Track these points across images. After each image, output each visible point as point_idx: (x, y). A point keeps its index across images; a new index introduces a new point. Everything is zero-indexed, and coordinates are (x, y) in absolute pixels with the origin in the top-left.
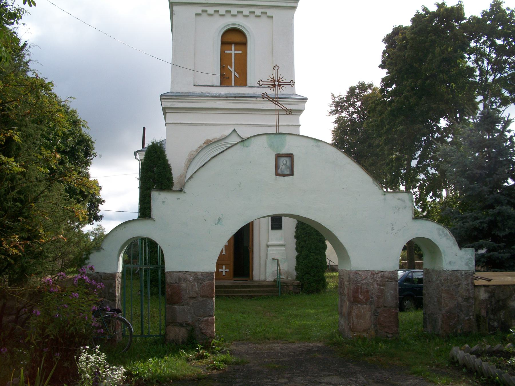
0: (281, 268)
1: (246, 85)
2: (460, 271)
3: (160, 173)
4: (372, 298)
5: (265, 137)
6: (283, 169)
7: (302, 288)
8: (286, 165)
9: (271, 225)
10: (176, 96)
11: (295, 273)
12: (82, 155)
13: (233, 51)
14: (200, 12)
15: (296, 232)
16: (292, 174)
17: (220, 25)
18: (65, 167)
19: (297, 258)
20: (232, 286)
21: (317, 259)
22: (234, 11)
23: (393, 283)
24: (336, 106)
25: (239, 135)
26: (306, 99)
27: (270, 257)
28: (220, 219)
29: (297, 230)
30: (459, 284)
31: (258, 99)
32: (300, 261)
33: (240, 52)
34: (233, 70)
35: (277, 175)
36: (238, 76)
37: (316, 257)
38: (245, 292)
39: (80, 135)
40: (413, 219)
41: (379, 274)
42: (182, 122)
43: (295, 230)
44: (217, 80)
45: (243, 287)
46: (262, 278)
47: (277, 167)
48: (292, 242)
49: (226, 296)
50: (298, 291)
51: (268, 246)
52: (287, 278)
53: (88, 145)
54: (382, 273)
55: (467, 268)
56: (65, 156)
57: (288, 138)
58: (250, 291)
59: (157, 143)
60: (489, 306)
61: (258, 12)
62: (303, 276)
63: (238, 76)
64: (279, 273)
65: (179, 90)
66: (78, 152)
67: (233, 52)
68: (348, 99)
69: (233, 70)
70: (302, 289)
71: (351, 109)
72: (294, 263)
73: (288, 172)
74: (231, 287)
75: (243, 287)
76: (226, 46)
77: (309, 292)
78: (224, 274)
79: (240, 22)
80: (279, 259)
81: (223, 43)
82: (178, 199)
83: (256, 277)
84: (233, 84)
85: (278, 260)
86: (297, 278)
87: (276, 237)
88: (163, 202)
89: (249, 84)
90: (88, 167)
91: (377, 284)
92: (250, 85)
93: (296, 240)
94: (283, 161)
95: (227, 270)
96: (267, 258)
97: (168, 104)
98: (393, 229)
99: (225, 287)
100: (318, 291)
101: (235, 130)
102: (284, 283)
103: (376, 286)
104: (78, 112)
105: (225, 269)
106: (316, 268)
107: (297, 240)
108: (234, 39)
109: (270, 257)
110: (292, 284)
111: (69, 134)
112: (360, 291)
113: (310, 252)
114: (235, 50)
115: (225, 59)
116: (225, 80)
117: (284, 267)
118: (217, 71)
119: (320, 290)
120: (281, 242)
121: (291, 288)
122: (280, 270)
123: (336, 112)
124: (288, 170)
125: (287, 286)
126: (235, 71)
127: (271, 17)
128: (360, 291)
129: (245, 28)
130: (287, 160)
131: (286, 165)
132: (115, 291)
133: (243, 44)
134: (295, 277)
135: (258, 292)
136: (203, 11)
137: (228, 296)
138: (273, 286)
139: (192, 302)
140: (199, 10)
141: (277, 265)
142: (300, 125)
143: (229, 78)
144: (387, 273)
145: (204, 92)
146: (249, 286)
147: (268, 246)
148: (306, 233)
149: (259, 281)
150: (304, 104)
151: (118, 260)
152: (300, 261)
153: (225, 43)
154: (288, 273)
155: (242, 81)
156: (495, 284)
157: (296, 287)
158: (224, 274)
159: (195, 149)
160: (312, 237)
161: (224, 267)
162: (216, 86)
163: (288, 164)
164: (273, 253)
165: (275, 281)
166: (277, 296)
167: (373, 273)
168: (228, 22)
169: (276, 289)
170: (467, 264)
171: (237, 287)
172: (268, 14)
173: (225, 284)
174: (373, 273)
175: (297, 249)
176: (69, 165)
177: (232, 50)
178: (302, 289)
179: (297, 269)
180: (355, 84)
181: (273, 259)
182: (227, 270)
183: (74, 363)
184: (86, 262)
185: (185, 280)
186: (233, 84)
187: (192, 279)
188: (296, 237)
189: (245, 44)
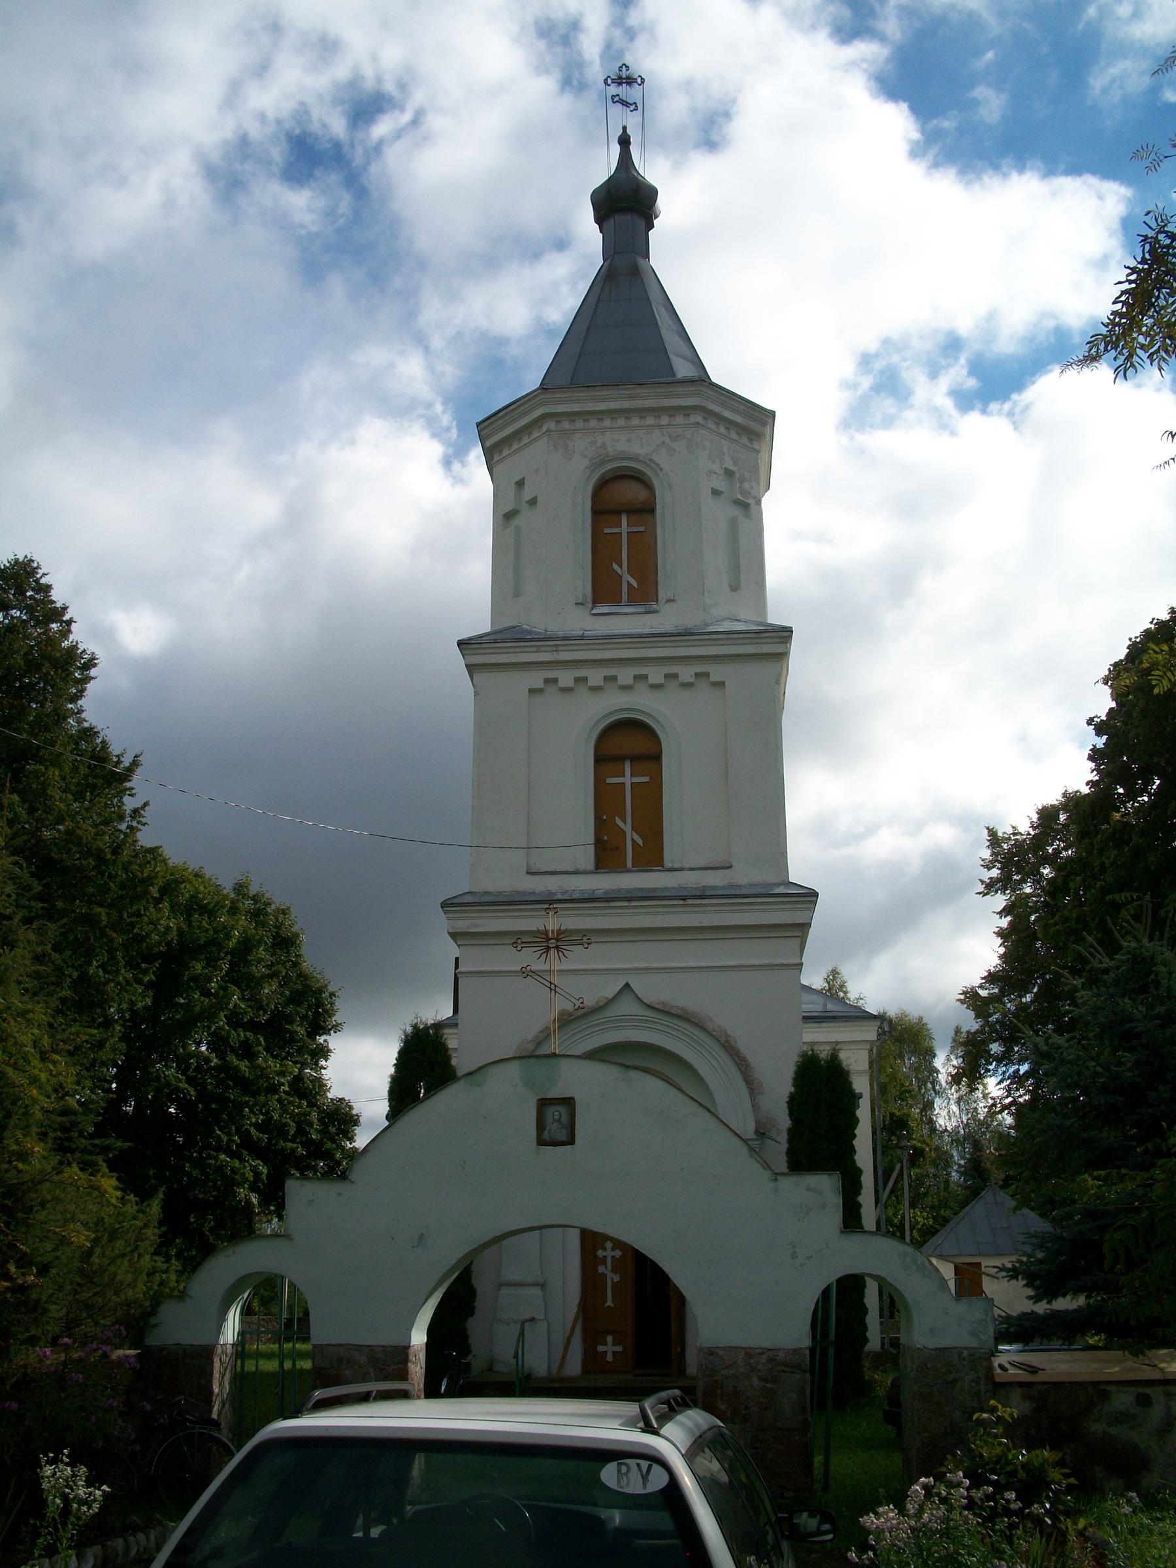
2: (959, 1351)
4: (747, 1408)
5: (516, 1064)
6: (554, 1130)
8: (559, 1121)
10: (481, 904)
12: (301, 1031)
14: (540, 685)
16: (571, 1141)
17: (596, 709)
18: (255, 1067)
22: (626, 675)
23: (798, 1376)
28: (421, 1237)
30: (955, 1380)
31: (690, 902)
33: (645, 779)
34: (627, 827)
35: (541, 1142)
36: (640, 842)
39: (300, 975)
40: (842, 1232)
41: (765, 1356)
44: (586, 857)
47: (541, 1125)
53: (320, 1004)
54: (771, 1353)
55: (974, 1343)
56: (255, 1034)
57: (564, 1064)
59: (427, 1028)
60: (1033, 1432)
61: (686, 673)
63: (640, 842)
65: (491, 887)
66: (291, 1023)
67: (627, 780)
69: (627, 827)
73: (563, 1136)
78: (610, 1358)
82: (340, 1194)
84: (629, 864)
88: (310, 1201)
90: (323, 1063)
91: (760, 1378)
94: (553, 1112)
95: (619, 1349)
97: (463, 925)
98: (794, 1256)
101: (627, 985)
103: (755, 1382)
104: (294, 912)
105: (605, 1344)
108: (628, 747)
112: (719, 1391)
115: (605, 802)
116: (607, 855)
118: (588, 833)
124: (564, 1132)
126: (633, 829)
127: (722, 684)
128: (719, 1391)
129: (658, 721)
130: (563, 1110)
131: (559, 1121)
132: (210, 1382)
136: (546, 681)
140: (536, 679)
143: (619, 849)
144: (781, 1355)
145: (553, 888)
151: (222, 1319)
155: (651, 856)
156: (1046, 1379)
158: (610, 1358)
159: (530, 1037)
161: (609, 1339)
163: (565, 1119)
167: (749, 1353)
170: (974, 1334)
172: (713, 678)
174: (749, 1353)
176: (266, 1060)
177: (624, 776)
182: (619, 1349)
183: (37, 1480)
184: (153, 1321)
186: (629, 864)
187: (363, 1360)
189: (656, 757)
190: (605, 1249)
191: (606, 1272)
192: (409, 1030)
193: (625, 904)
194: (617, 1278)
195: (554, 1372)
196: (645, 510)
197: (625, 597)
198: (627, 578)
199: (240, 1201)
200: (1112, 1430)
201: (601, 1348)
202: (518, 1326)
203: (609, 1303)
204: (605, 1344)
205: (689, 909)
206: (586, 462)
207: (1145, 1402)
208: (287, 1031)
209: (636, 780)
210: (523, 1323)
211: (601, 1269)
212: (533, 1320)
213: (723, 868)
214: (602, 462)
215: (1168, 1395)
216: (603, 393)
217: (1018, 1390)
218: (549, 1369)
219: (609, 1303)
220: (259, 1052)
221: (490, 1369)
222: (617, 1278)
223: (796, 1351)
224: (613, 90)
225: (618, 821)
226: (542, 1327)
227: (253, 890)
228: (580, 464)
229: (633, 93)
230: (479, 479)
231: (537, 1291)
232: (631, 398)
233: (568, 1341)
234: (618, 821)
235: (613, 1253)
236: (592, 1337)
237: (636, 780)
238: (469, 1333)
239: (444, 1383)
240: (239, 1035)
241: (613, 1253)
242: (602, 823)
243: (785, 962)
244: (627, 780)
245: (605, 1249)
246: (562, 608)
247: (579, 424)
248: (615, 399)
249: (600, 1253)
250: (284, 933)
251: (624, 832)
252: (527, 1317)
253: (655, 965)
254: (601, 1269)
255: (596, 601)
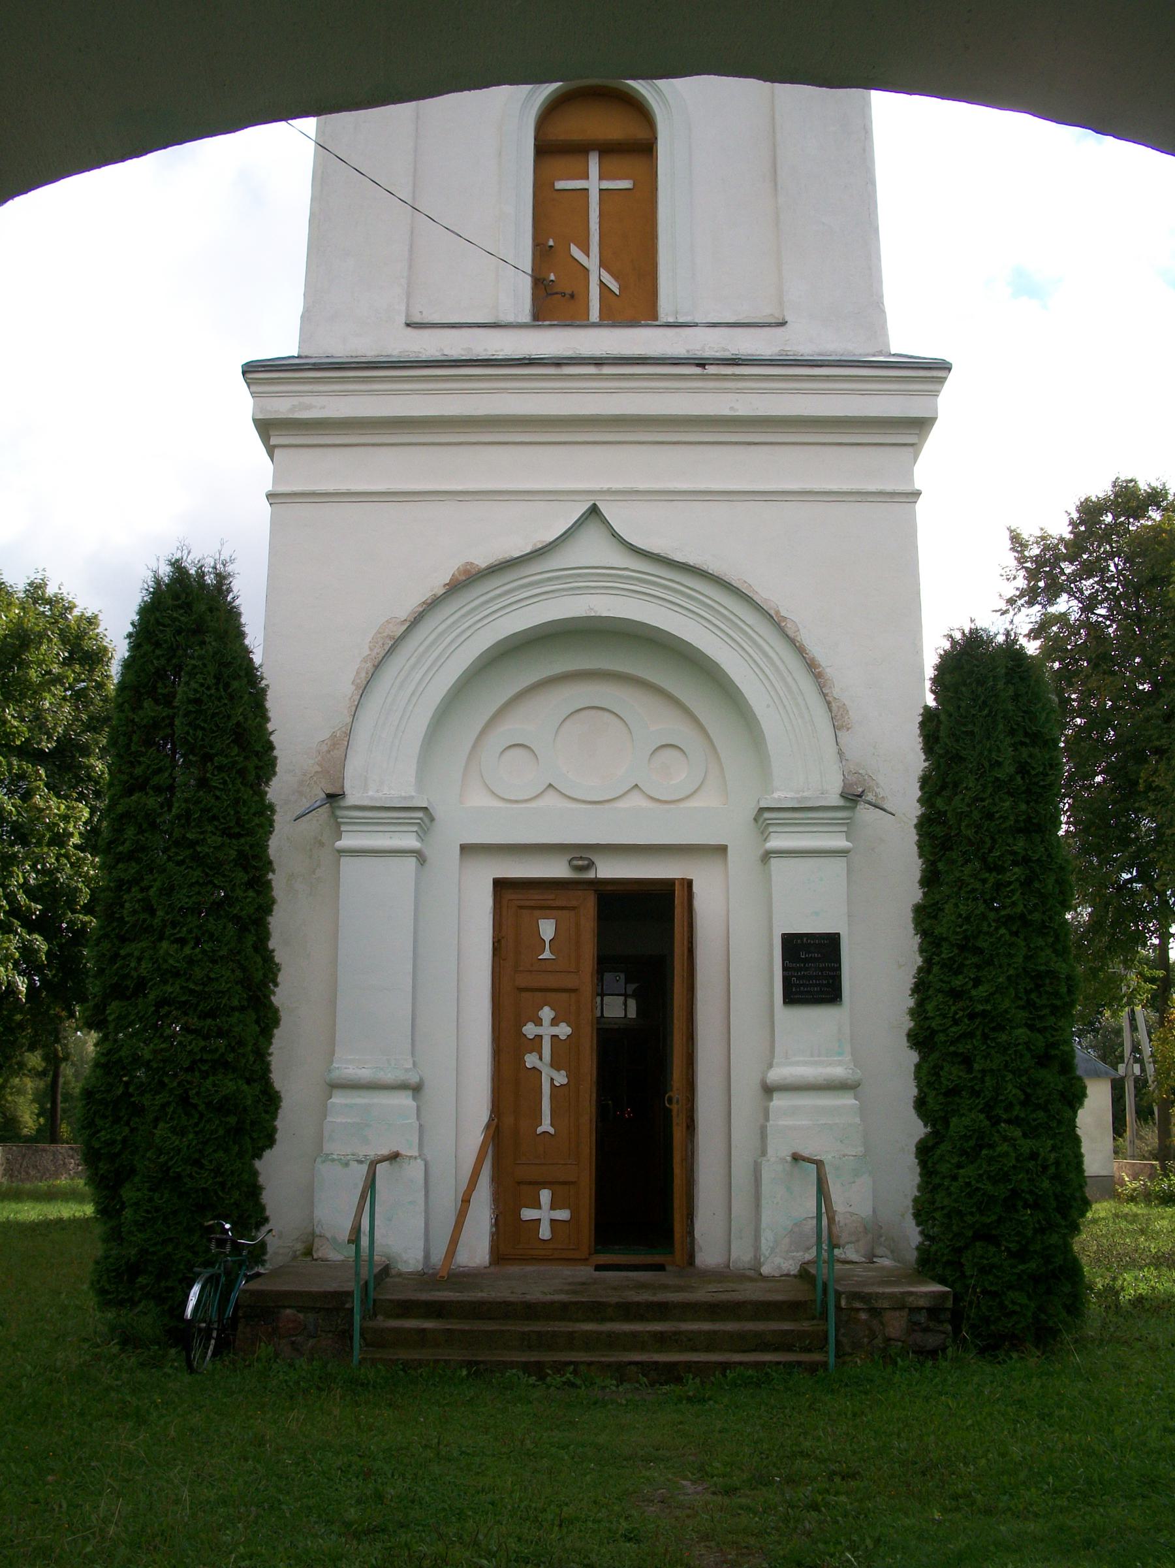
0: (839, 1206)
1: (654, 316)
3: (198, 701)
7: (957, 1318)
9: (786, 981)
11: (912, 1235)
13: (592, 180)
15: (918, 1012)
19: (924, 1151)
20: (565, 1306)
21: (1034, 1156)
24: (1032, 575)
25: (615, 535)
26: (946, 367)
27: (779, 1149)
29: (920, 1004)
31: (711, 370)
32: (943, 1168)
33: (626, 184)
34: (592, 263)
36: (614, 286)
37: (1026, 1146)
38: (635, 1342)
42: (343, 487)
43: (911, 1003)
44: (516, 295)
45: (629, 1311)
46: (741, 1255)
48: (902, 1062)
49: (527, 1368)
50: (932, 1341)
51: (769, 1090)
52: (871, 1258)
58: (662, 1341)
62: (959, 1251)
63: (614, 286)
64: (827, 1231)
66: (88, 756)
68: (1076, 547)
69: (592, 263)
70: (957, 1330)
71: (1088, 585)
72: (905, 1179)
74: (561, 1311)
75: (629, 1311)
77: (994, 1344)
78: (545, 1232)
80: (826, 1158)
81: (545, 150)
83: (708, 1255)
84: (594, 315)
85: (819, 1164)
86: (927, 1264)
87: (809, 1042)
89: (666, 308)
92: (671, 320)
93: (914, 1057)
95: (563, 1215)
96: (764, 1153)
97: (282, 407)
99: (531, 1311)
100: (1044, 1336)
101: (594, 510)
102: (855, 1296)
105: (537, 1205)
106: (1035, 1206)
107: (923, 1059)
109: (779, 1149)
110: (899, 1304)
111: (41, 684)
113: (995, 1121)
114: (601, 178)
116: (553, 299)
117: (853, 1200)
119: (1054, 1333)
120: (838, 1071)
121: (896, 1325)
122: (831, 1220)
123: (1031, 595)
125: (875, 1312)
126: (602, 264)
134: (912, 1256)
135: (712, 1342)
137: (537, 1370)
138: (793, 1309)
141: (814, 1190)
142: (918, 494)
146: (662, 1310)
147: (769, 1090)
148: (972, 1016)
149: (722, 1275)
150: (935, 394)
152: (943, 1168)
154: (875, 1233)
155: (636, 301)
157: (922, 1318)
158: (545, 1232)
160: (1003, 1037)
161: (545, 1196)
164: (799, 1124)
165: (805, 1275)
166: (812, 1368)
169: (808, 1328)
171: (596, 1311)
173: (537, 1293)
175: (920, 1105)
177: (586, 177)
178: (957, 1330)
179: (922, 1212)
180: (1100, 489)
181: (796, 1158)
182: (563, 1215)
186: (594, 315)
188: (920, 1039)
190: (538, 1022)
191: (538, 1064)
192: (165, 571)
193: (592, 370)
194: (561, 1079)
195: (438, 1256)
201: (528, 1214)
202: (364, 1168)
203: (546, 1126)
204: (537, 1205)
205: (711, 384)
208: (81, 766)
209: (607, 185)
210: (373, 1165)
211: (531, 1060)
212: (394, 1157)
213: (769, 325)
218: (427, 1256)
219: (546, 1126)
220: (38, 788)
221: (308, 1252)
222: (561, 1079)
225: (575, 251)
226: (415, 1171)
227: (50, 591)
231: (405, 1100)
233: (466, 1201)
234: (575, 251)
235: (555, 1031)
236: (511, 1193)
238: (262, 1180)
239: (196, 1289)
240: (10, 765)
241: (555, 1031)
243: (889, 488)
244: (593, 184)
245: (538, 1022)
249: (530, 1030)
250: (87, 645)
251: (586, 270)
252: (385, 1152)
253: (642, 486)
254: (531, 1060)
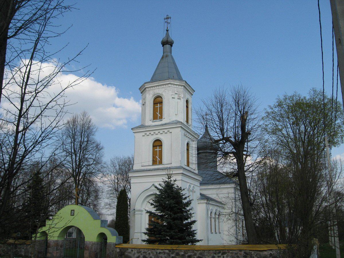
6: (72, 214)
14: (144, 135)
22: (157, 132)
31: (163, 170)
33: (155, 150)
34: (158, 158)
35: (71, 215)
61: (166, 131)
69: (158, 158)
76: (155, 147)
79: (159, 137)
94: (73, 212)
103: (90, 246)
108: (158, 144)
115: (154, 154)
116: (154, 162)
133: (161, 146)
139: (52, 247)
140: (143, 134)
143: (156, 161)
153: (154, 146)
155: (161, 163)
162: (150, 166)
168: (155, 137)
185: (51, 242)
187: (52, 242)
196: (161, 103)
197: (158, 118)
198: (159, 115)
199: (185, 209)
200: (128, 254)
206: (152, 95)
207: (132, 251)
209: (157, 150)
214: (155, 95)
215: (135, 250)
216: (154, 83)
217: (118, 248)
223: (95, 242)
224: (166, 20)
228: (151, 96)
229: (169, 20)
230: (114, 107)
232: (159, 83)
234: (156, 157)
237: (157, 150)
242: (154, 157)
244: (158, 149)
246: (149, 121)
247: (151, 88)
248: (157, 83)
255: (154, 119)
